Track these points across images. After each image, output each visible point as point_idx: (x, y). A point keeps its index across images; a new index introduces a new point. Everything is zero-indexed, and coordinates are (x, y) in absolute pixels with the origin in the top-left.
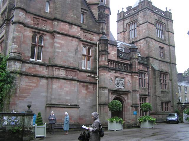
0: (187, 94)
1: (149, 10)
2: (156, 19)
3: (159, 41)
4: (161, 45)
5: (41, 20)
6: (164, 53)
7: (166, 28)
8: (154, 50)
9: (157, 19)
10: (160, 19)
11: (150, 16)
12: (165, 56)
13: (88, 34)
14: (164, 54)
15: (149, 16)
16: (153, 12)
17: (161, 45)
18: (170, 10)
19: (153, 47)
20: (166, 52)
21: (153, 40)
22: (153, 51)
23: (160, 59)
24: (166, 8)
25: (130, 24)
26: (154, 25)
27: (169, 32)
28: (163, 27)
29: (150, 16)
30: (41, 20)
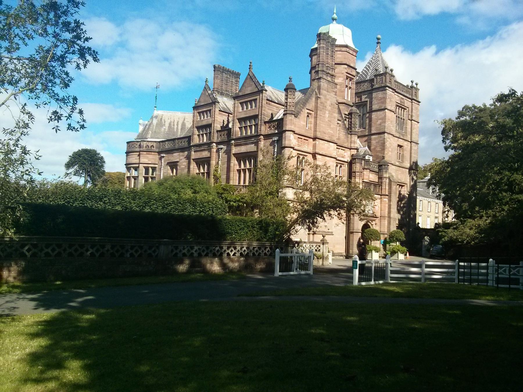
0: (438, 213)
1: (390, 90)
2: (397, 103)
3: (398, 136)
4: (401, 142)
5: (304, 139)
6: (403, 154)
7: (409, 114)
8: (391, 152)
9: (397, 102)
10: (402, 101)
11: (390, 99)
12: (403, 158)
13: (340, 150)
14: (403, 156)
15: (389, 98)
16: (394, 91)
17: (401, 142)
18: (417, 84)
19: (390, 147)
20: (405, 152)
21: (390, 136)
22: (390, 153)
23: (397, 164)
24: (412, 82)
25: (362, 105)
26: (393, 112)
27: (410, 141)
28: (405, 113)
29: (390, 99)
30: (304, 139)
